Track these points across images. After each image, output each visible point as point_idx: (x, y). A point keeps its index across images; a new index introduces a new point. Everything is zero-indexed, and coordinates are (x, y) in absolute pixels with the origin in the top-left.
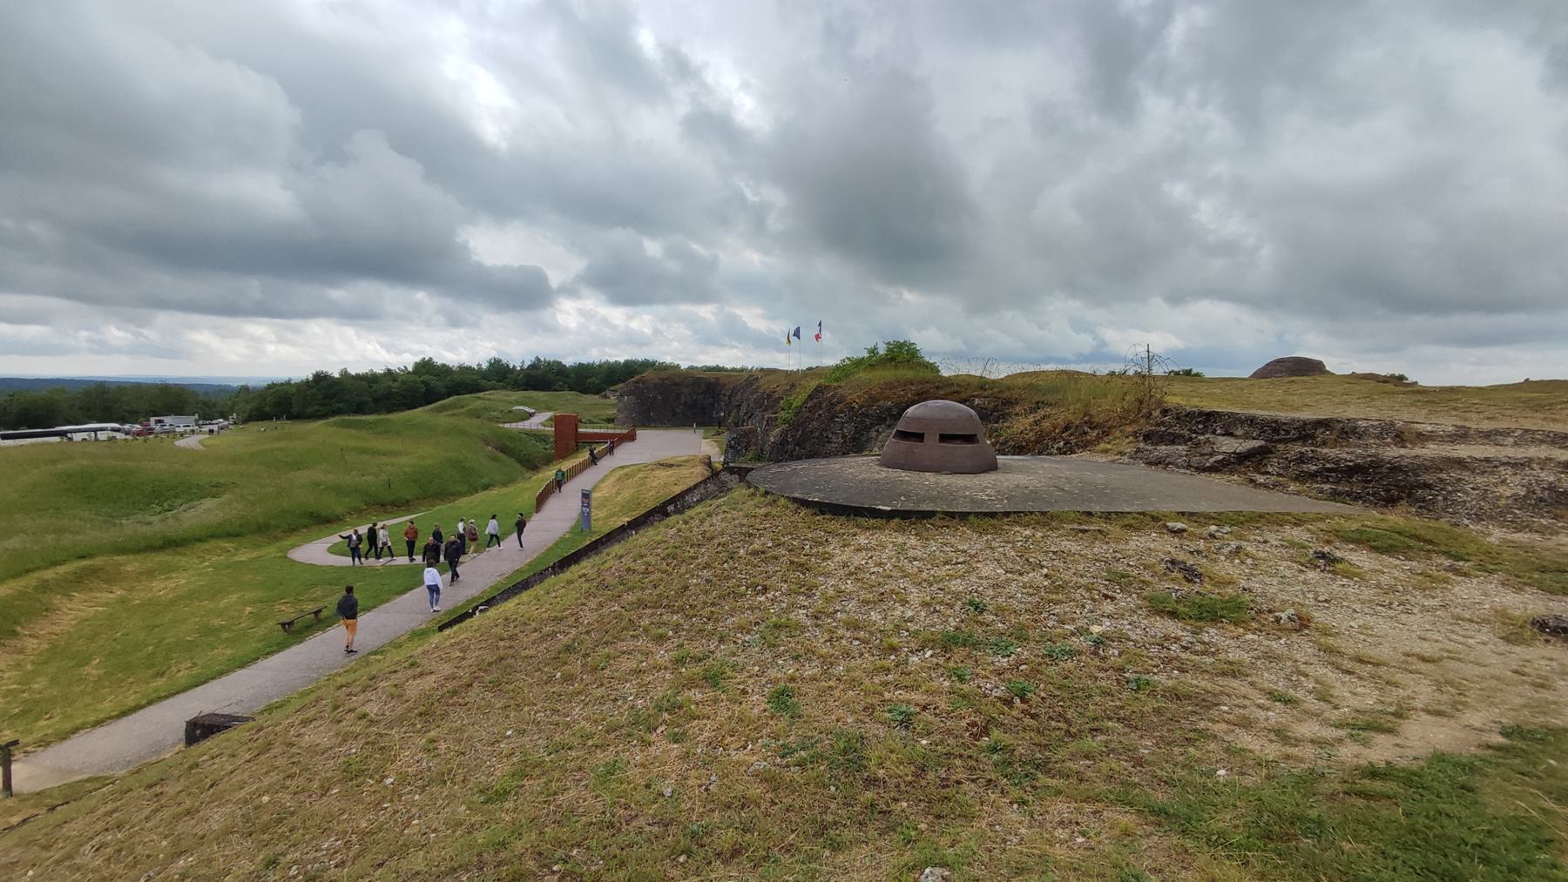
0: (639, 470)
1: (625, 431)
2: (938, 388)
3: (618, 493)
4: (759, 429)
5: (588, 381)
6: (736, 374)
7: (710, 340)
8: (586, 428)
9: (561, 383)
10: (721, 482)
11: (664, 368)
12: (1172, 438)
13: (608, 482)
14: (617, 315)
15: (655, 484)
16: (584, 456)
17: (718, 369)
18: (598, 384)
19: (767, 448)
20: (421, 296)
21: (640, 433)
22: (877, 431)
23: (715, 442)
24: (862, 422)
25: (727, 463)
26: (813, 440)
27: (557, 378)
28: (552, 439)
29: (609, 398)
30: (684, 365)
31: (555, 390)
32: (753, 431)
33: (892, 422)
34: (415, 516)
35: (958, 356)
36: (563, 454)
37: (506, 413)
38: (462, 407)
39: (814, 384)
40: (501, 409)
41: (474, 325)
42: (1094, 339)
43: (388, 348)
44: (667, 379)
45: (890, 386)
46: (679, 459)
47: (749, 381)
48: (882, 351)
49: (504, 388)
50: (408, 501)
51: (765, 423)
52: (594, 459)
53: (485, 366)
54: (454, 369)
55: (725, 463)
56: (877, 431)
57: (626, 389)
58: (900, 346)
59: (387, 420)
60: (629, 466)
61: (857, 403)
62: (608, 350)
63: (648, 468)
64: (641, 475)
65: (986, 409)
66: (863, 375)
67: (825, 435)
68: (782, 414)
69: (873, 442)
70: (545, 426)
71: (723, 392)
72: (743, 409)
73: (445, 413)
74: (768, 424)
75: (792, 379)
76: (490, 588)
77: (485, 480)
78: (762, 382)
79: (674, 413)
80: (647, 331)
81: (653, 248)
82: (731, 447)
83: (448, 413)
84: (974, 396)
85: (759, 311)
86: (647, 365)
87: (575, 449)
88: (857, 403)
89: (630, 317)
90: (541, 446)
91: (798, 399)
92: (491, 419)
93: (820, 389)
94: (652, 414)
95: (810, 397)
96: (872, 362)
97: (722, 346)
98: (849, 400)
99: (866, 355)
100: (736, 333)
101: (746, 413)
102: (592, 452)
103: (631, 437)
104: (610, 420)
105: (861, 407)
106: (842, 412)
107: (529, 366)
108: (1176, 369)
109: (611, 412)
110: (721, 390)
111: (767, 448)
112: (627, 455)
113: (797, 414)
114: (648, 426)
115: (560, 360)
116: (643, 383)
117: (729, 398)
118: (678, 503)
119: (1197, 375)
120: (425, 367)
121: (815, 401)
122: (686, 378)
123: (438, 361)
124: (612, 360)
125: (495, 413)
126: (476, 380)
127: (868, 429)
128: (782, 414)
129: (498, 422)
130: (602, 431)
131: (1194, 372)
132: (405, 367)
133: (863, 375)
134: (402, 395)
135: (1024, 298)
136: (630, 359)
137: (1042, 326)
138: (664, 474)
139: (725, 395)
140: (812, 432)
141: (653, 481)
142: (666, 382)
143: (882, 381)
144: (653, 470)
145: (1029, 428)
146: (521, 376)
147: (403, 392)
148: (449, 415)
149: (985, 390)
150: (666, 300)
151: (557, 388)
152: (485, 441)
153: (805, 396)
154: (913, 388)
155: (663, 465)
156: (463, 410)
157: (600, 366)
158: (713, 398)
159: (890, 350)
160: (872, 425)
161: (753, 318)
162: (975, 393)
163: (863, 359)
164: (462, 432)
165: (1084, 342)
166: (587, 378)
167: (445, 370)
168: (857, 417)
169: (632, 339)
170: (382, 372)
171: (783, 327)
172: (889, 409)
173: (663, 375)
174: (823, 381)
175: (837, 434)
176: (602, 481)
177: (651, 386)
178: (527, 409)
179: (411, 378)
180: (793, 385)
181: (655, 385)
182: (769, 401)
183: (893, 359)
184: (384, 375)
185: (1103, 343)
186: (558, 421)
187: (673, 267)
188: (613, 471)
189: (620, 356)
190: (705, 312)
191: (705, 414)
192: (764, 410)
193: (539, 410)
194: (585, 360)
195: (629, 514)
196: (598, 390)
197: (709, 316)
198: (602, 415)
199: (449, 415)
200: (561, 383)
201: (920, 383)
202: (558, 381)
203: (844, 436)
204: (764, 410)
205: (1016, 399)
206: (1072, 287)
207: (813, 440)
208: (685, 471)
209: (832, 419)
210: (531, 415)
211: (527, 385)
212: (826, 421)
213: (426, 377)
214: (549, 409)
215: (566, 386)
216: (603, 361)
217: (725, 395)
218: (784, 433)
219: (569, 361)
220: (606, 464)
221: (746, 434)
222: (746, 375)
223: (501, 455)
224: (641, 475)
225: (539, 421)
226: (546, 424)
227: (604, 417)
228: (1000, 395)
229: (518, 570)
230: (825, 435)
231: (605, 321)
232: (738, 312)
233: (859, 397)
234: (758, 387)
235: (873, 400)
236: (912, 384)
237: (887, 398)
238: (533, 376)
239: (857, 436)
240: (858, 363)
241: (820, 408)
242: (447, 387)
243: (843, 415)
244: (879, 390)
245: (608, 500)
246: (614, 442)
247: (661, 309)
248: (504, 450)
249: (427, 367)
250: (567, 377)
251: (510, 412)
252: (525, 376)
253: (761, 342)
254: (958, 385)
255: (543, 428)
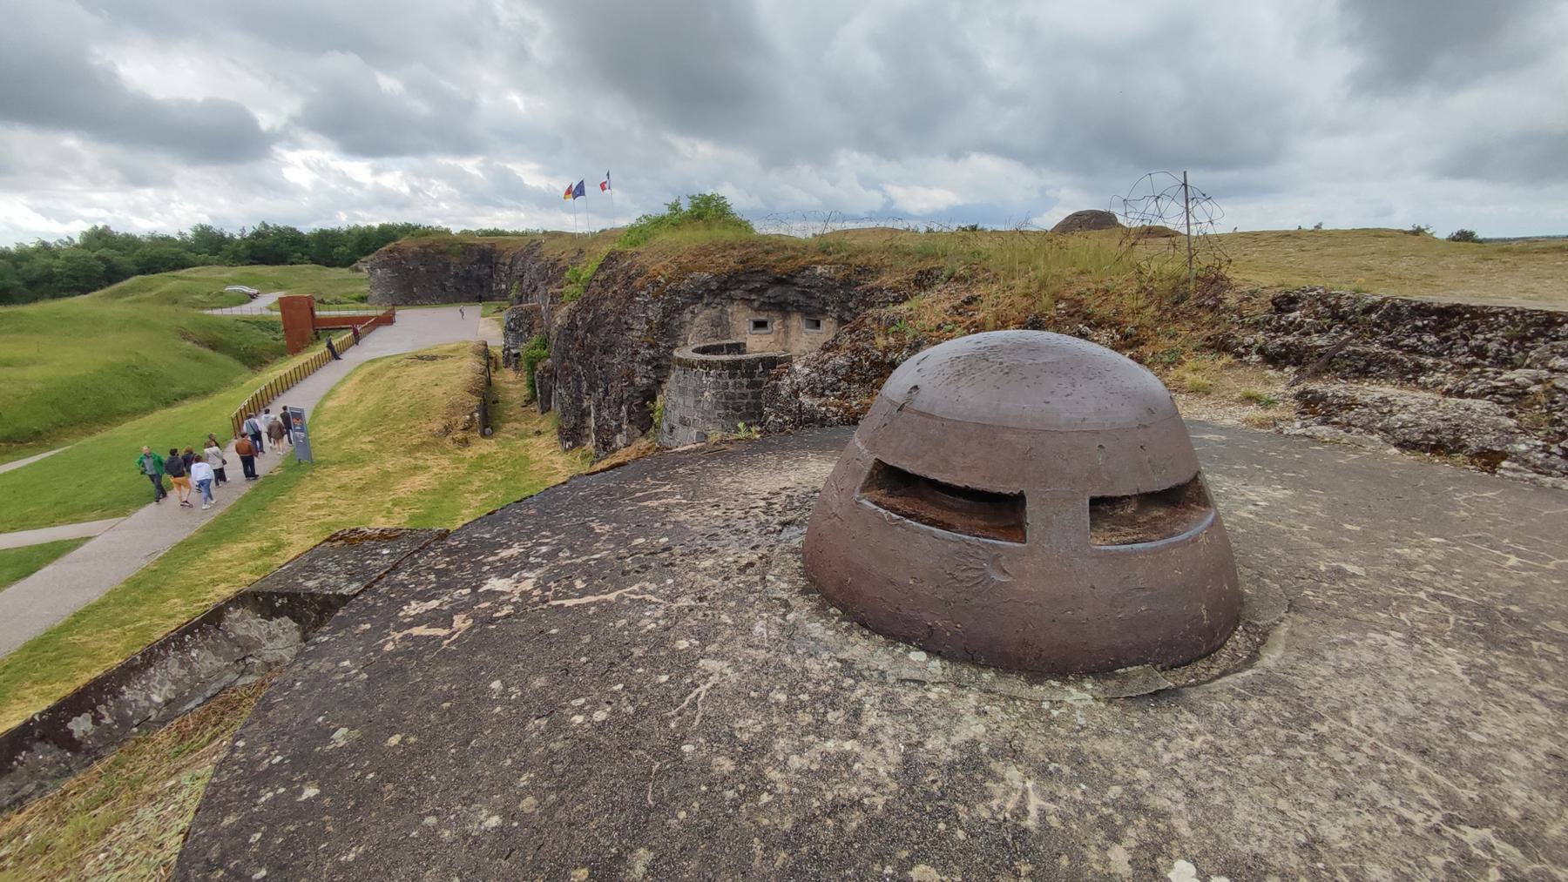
0: (389, 367)
1: (380, 312)
2: (767, 253)
3: (360, 401)
4: (543, 308)
5: (335, 250)
6: (515, 238)
7: (482, 200)
8: (348, 309)
9: (300, 255)
10: (234, 642)
11: (428, 232)
12: (1362, 364)
13: (349, 385)
14: (359, 169)
15: (408, 386)
16: (321, 349)
17: (496, 233)
18: (349, 255)
19: (553, 332)
20: (70, 141)
21: (403, 315)
22: (693, 312)
23: (497, 320)
24: (671, 301)
25: (509, 349)
26: (609, 327)
27: (292, 248)
28: (282, 328)
29: (361, 271)
30: (456, 229)
31: (292, 263)
32: (538, 310)
33: (710, 300)
34: (52, 453)
35: (767, 217)
36: (295, 349)
37: (216, 296)
38: (150, 290)
39: (606, 249)
40: (207, 291)
41: (166, 183)
42: (884, 196)
43: (46, 213)
44: (429, 246)
45: (704, 251)
46: (446, 348)
47: (531, 244)
48: (686, 206)
49: (219, 263)
50: (38, 433)
51: (549, 300)
52: (335, 355)
53: (190, 234)
54: (144, 240)
55: (506, 349)
56: (693, 312)
57: (377, 261)
58: (707, 200)
59: (20, 313)
60: (380, 359)
61: (663, 276)
62: (360, 213)
63: (400, 364)
64: (392, 373)
65: (832, 280)
66: (666, 237)
67: (623, 320)
68: (569, 289)
69: (688, 327)
70: (271, 310)
71: (501, 261)
72: (526, 282)
73: (126, 299)
74: (552, 302)
75: (580, 244)
76: (126, 582)
77: (178, 389)
78: (544, 248)
79: (444, 288)
80: (405, 190)
81: (389, 84)
82: (512, 330)
83: (130, 298)
84: (815, 262)
85: (533, 166)
86: (408, 230)
87: (314, 337)
88: (663, 276)
89: (377, 172)
90: (269, 336)
91: (588, 269)
92: (194, 305)
93: (612, 258)
94: (415, 289)
95: (602, 267)
96: (674, 220)
97: (501, 206)
98: (651, 273)
99: (667, 212)
100: (514, 192)
101: (529, 286)
102: (330, 346)
103: (388, 320)
104: (363, 299)
105: (668, 281)
106: (643, 288)
107: (253, 234)
108: (963, 226)
109: (364, 289)
110: (499, 257)
111: (553, 332)
112: (381, 344)
113: (587, 289)
114: (412, 305)
115: (292, 226)
116: (399, 253)
117: (510, 268)
118: (102, 709)
119: (982, 230)
120: (100, 238)
121: (608, 271)
122: (454, 245)
123: (119, 228)
124: (363, 225)
125: (198, 297)
126: (179, 253)
127: (679, 310)
128: (569, 289)
129: (203, 308)
130: (352, 313)
131: (979, 227)
132: (69, 238)
133: (666, 237)
134: (68, 276)
135: (818, 152)
136: (386, 223)
137: (833, 183)
138: (421, 371)
139: (504, 264)
140: (606, 315)
141: (407, 382)
142: (429, 250)
143: (694, 245)
144: (407, 366)
145: (949, 320)
146: (243, 246)
147: (70, 273)
148: (130, 302)
149: (830, 254)
150: (420, 150)
151: (294, 260)
152: (182, 334)
153: (594, 266)
154: (736, 254)
155: (421, 358)
156: (147, 295)
157: (349, 232)
158: (491, 267)
159: (696, 206)
160: (685, 305)
161: (529, 174)
162: (816, 259)
163: (663, 218)
164: (144, 325)
165: (871, 200)
166: (333, 247)
167: (129, 244)
168: (664, 294)
169: (384, 198)
170: (32, 246)
171: (561, 186)
172: (706, 283)
173: (425, 241)
174: (616, 245)
175: (638, 318)
176: (343, 382)
177: (410, 255)
178: (247, 289)
179: (81, 253)
180: (581, 251)
181: (415, 254)
182: (553, 272)
183: (699, 217)
184: (37, 250)
185: (891, 202)
186: (284, 304)
187: (422, 108)
188: (359, 367)
189: (373, 219)
190: (470, 166)
191: (482, 287)
192: (547, 283)
193: (267, 290)
194: (329, 225)
195: (372, 432)
196: (348, 262)
197: (476, 172)
198: (352, 293)
199: (130, 302)
200: (300, 255)
201: (743, 246)
202: (294, 251)
203: (649, 322)
204: (547, 283)
205: (876, 266)
206: (870, 142)
207: (609, 327)
208: (449, 366)
209: (630, 298)
210: (253, 297)
211: (254, 258)
212: (624, 300)
213: (103, 252)
214: (280, 287)
215: (306, 257)
216: (351, 226)
217: (504, 264)
218: (572, 315)
219: (307, 228)
220: (352, 357)
221: (527, 314)
222: (527, 240)
223: (208, 352)
224: (392, 373)
225: (265, 305)
226: (273, 307)
227: (355, 295)
228: (851, 260)
229: (180, 545)
230: (623, 320)
231: (345, 179)
232: (509, 166)
233: (665, 268)
234: (542, 254)
235: (684, 271)
236: (734, 248)
237: (702, 269)
238: (259, 247)
239: (667, 320)
240: (659, 222)
241: (615, 282)
242: (138, 264)
243: (645, 293)
244: (691, 258)
245: (345, 411)
246: (358, 329)
247: (414, 161)
248: (214, 345)
249: (104, 238)
250: (307, 246)
251: (222, 294)
252: (247, 248)
253: (543, 201)
254: (794, 249)
255: (269, 313)
